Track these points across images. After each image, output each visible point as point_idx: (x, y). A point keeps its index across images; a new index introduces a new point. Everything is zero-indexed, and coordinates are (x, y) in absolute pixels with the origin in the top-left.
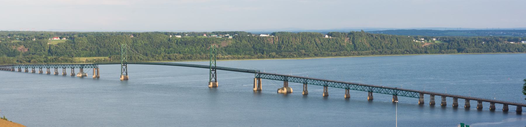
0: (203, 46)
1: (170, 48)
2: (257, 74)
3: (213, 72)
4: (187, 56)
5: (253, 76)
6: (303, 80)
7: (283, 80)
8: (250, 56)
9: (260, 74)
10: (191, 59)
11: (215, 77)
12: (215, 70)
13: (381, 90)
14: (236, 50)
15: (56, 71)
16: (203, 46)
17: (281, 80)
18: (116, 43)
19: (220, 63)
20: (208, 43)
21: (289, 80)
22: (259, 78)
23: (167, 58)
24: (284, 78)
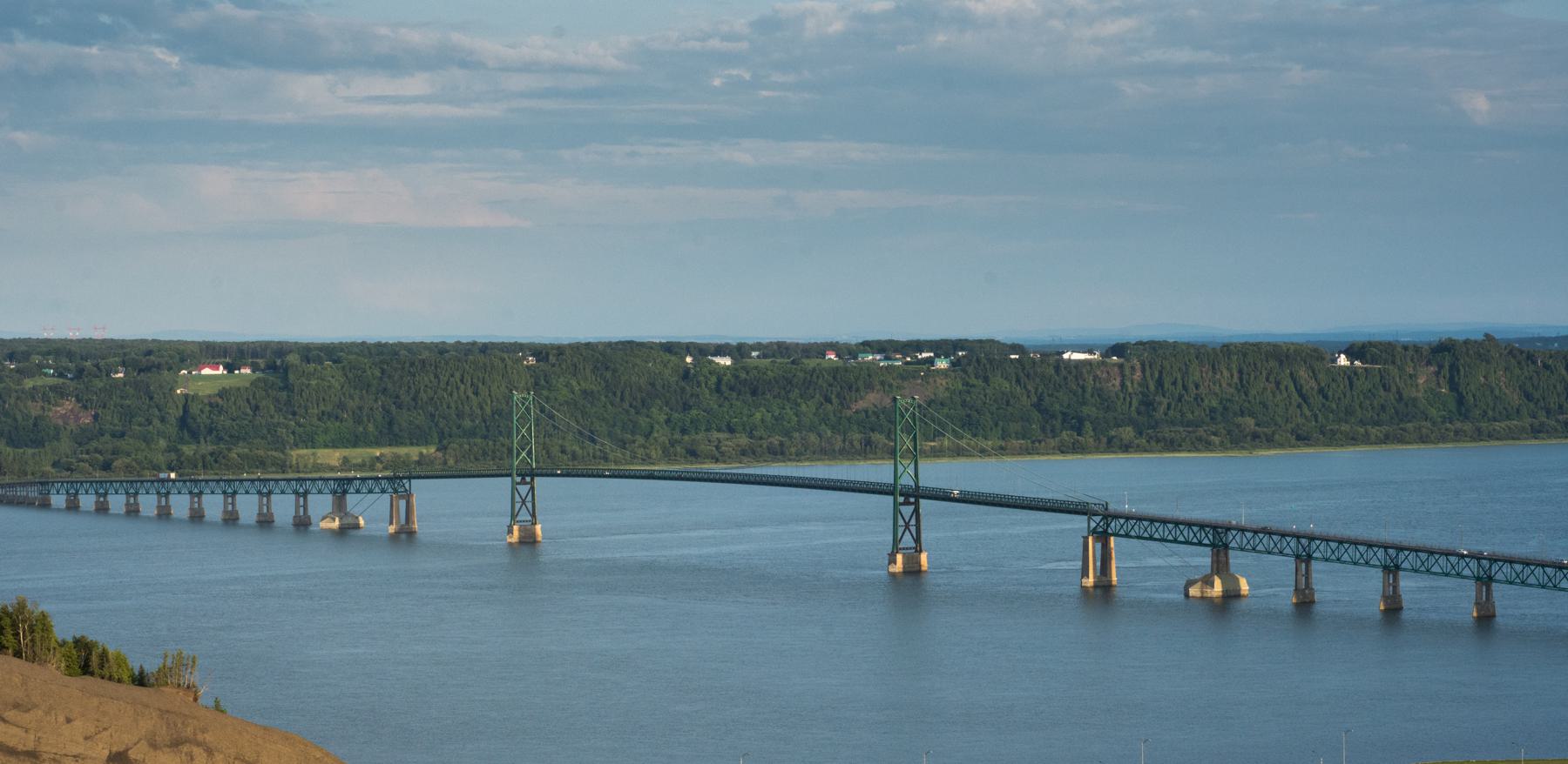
0: (828, 400)
1: (690, 408)
2: (1097, 519)
3: (907, 511)
4: (765, 444)
5: (1080, 523)
6: (1292, 544)
7: (1206, 541)
8: (762, 409)
9: (1109, 516)
11: (913, 529)
12: (917, 504)
13: (1527, 571)
15: (230, 508)
16: (828, 400)
17: (1200, 544)
18: (462, 387)
19: (935, 473)
20: (850, 388)
21: (1233, 544)
22: (1103, 537)
24: (1211, 537)
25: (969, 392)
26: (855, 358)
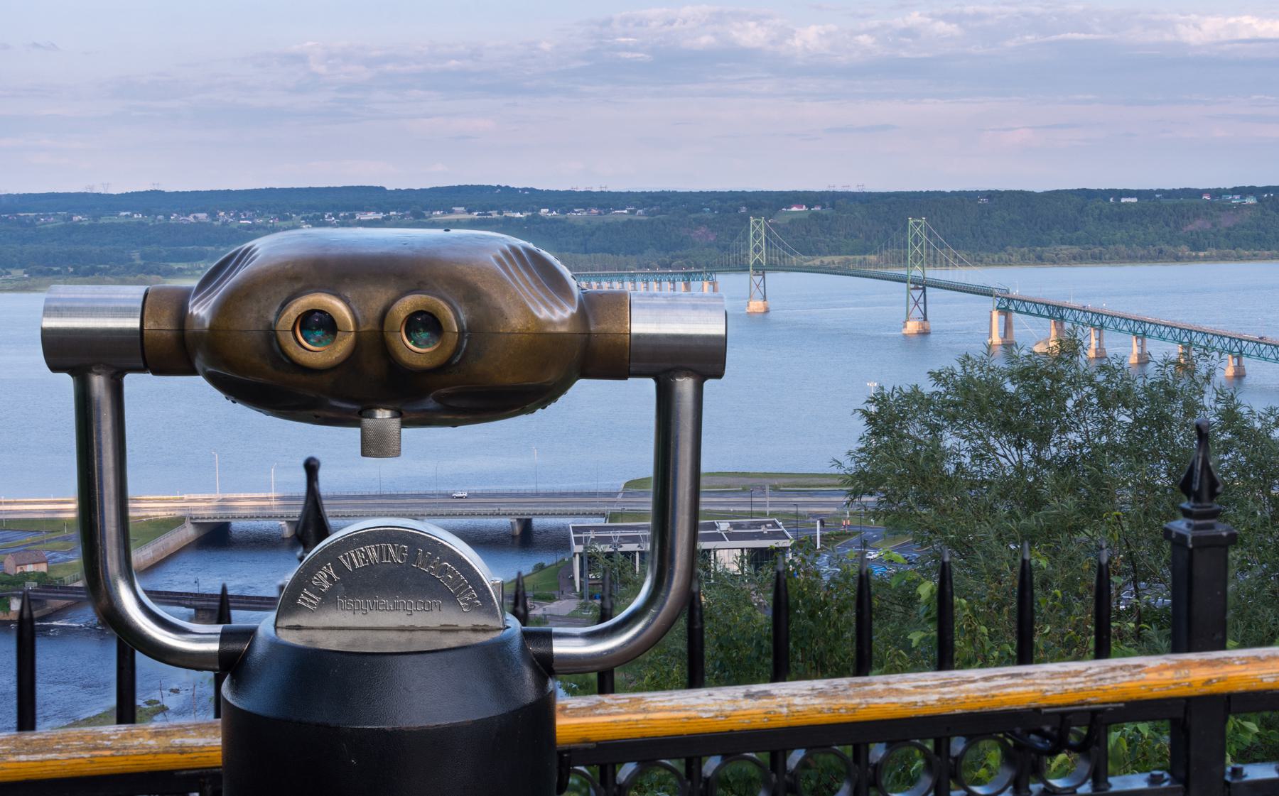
0: (1167, 225)
4: (1089, 252)
5: (989, 303)
10: (1101, 259)
11: (922, 306)
14: (1259, 234)
16: (1167, 225)
18: (934, 217)
19: (933, 274)
20: (1183, 217)
22: (1005, 311)
23: (1034, 257)
25: (1264, 219)
26: (1221, 197)
